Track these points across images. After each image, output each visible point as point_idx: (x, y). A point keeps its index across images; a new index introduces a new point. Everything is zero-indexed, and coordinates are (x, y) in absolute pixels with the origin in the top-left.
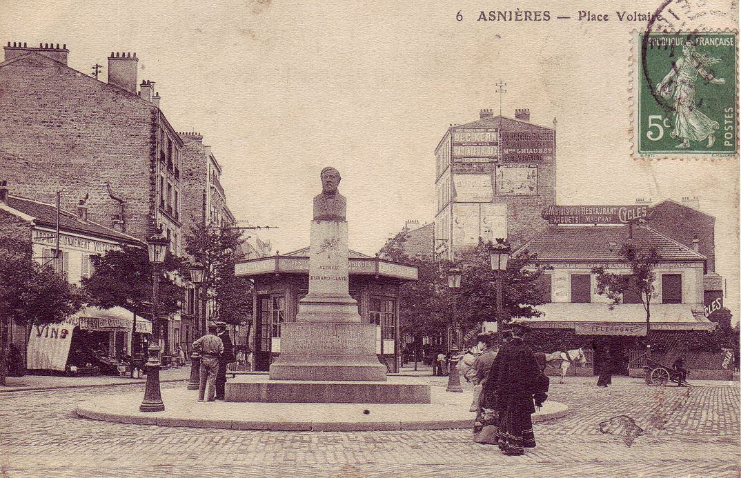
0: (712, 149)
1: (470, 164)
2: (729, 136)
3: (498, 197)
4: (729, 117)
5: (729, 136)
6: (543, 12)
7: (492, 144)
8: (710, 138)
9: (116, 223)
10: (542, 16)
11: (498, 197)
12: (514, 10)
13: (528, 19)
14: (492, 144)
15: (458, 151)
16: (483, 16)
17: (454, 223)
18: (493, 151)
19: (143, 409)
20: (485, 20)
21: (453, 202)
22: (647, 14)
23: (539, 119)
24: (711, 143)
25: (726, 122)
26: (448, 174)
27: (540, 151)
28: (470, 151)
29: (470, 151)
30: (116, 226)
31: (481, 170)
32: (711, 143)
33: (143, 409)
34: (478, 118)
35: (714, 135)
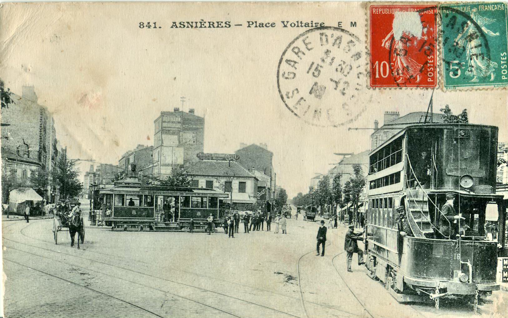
0: (493, 82)
1: (169, 131)
2: (504, 72)
3: (180, 145)
4: (504, 59)
5: (504, 72)
6: (224, 22)
7: (179, 122)
8: (492, 74)
9: (25, 154)
10: (223, 25)
11: (180, 145)
12: (198, 20)
13: (211, 26)
14: (179, 122)
15: (165, 125)
16: (174, 25)
17: (162, 154)
18: (179, 126)
19: (91, 225)
20: (177, 27)
21: (161, 146)
22: (310, 23)
23: (198, 113)
24: (492, 78)
25: (502, 62)
26: (160, 134)
27: (198, 127)
28: (170, 125)
29: (170, 125)
30: (25, 155)
31: (173, 134)
32: (492, 78)
33: (91, 225)
34: (173, 111)
35: (494, 72)
